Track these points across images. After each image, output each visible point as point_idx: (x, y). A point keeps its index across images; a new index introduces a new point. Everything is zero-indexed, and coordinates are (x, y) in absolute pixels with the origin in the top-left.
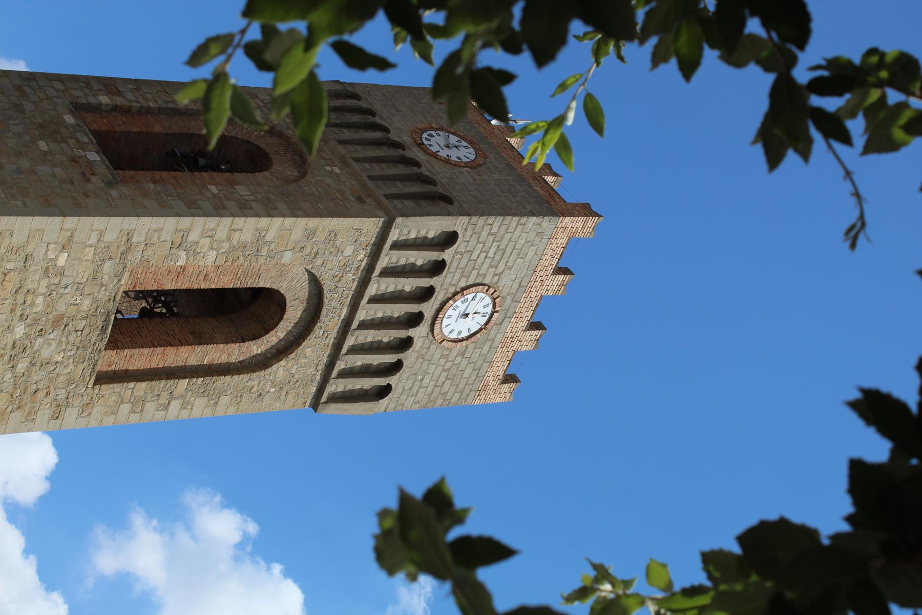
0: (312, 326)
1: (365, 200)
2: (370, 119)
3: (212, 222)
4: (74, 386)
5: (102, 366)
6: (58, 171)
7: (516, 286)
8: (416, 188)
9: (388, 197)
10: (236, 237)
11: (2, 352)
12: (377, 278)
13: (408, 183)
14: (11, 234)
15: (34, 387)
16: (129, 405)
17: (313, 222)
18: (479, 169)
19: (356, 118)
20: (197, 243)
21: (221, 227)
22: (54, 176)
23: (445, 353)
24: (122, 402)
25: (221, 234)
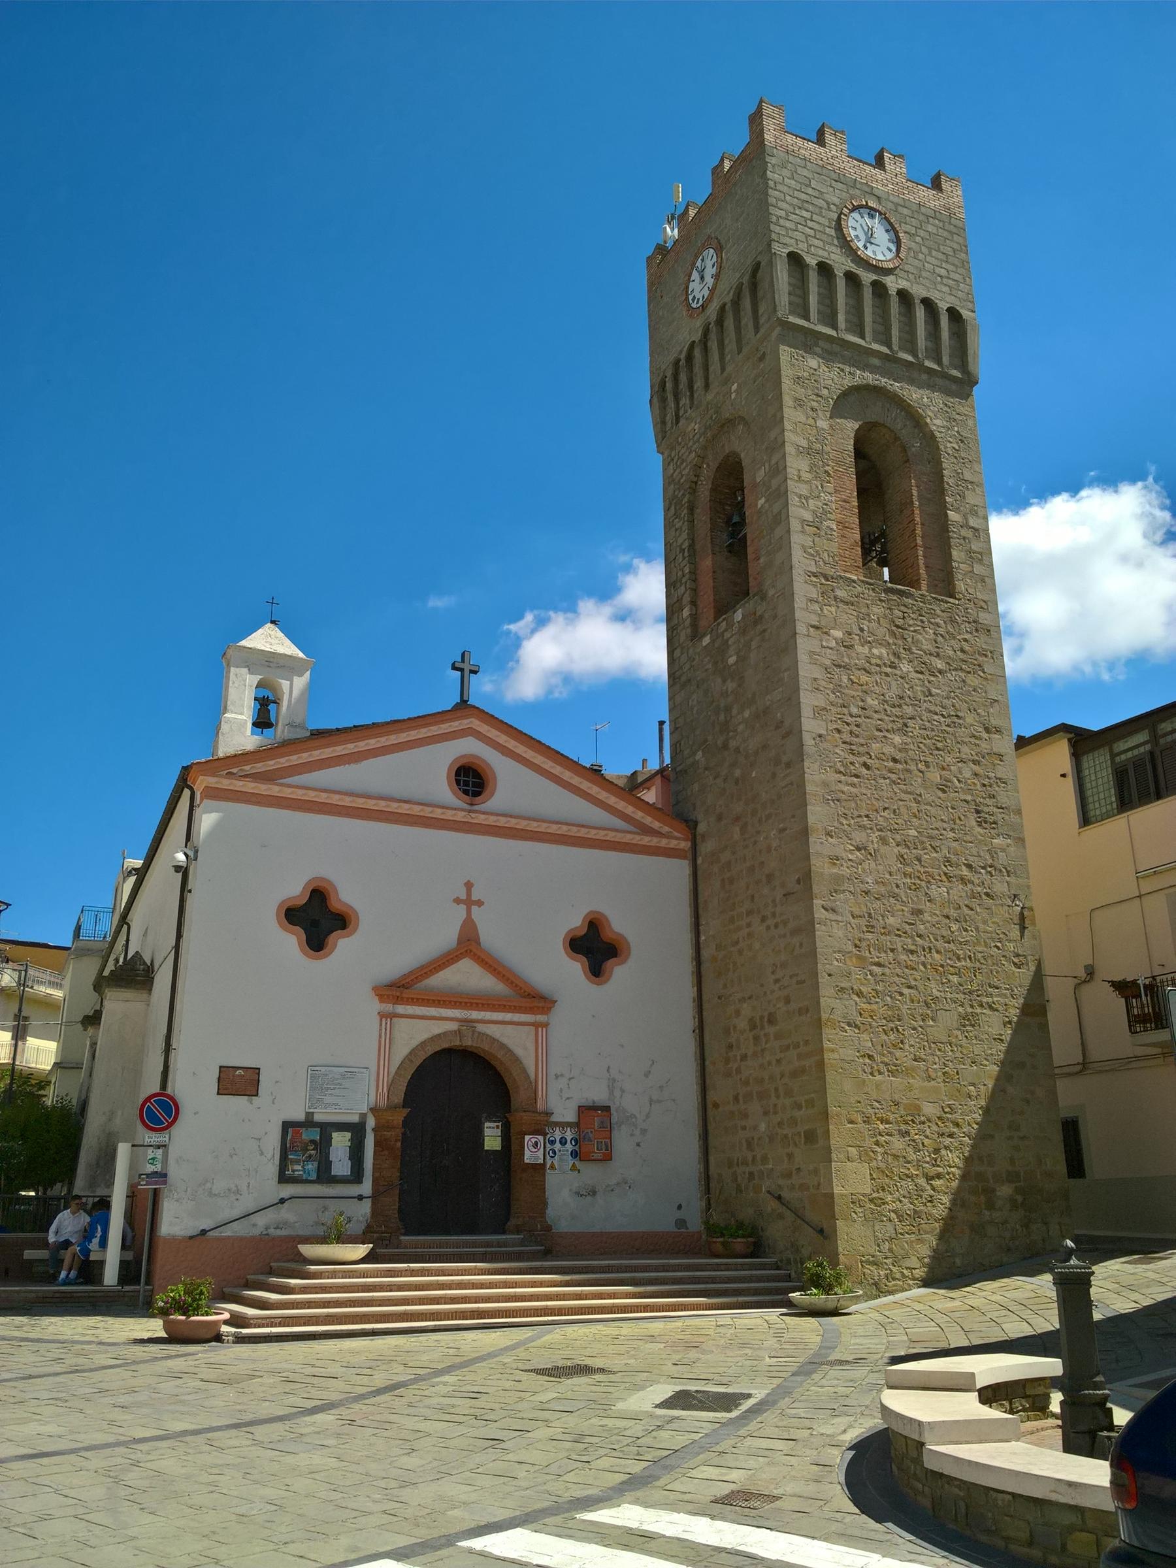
0: (890, 394)
1: (762, 353)
2: (683, 362)
3: (793, 500)
4: (957, 617)
7: (839, 185)
8: (747, 303)
9: (757, 329)
10: (806, 476)
12: (839, 331)
13: (742, 313)
14: (815, 679)
15: (959, 653)
16: (975, 565)
17: (787, 400)
18: (723, 242)
19: (683, 377)
20: (814, 512)
21: (797, 490)
22: (759, 647)
23: (912, 255)
24: (972, 572)
25: (804, 490)
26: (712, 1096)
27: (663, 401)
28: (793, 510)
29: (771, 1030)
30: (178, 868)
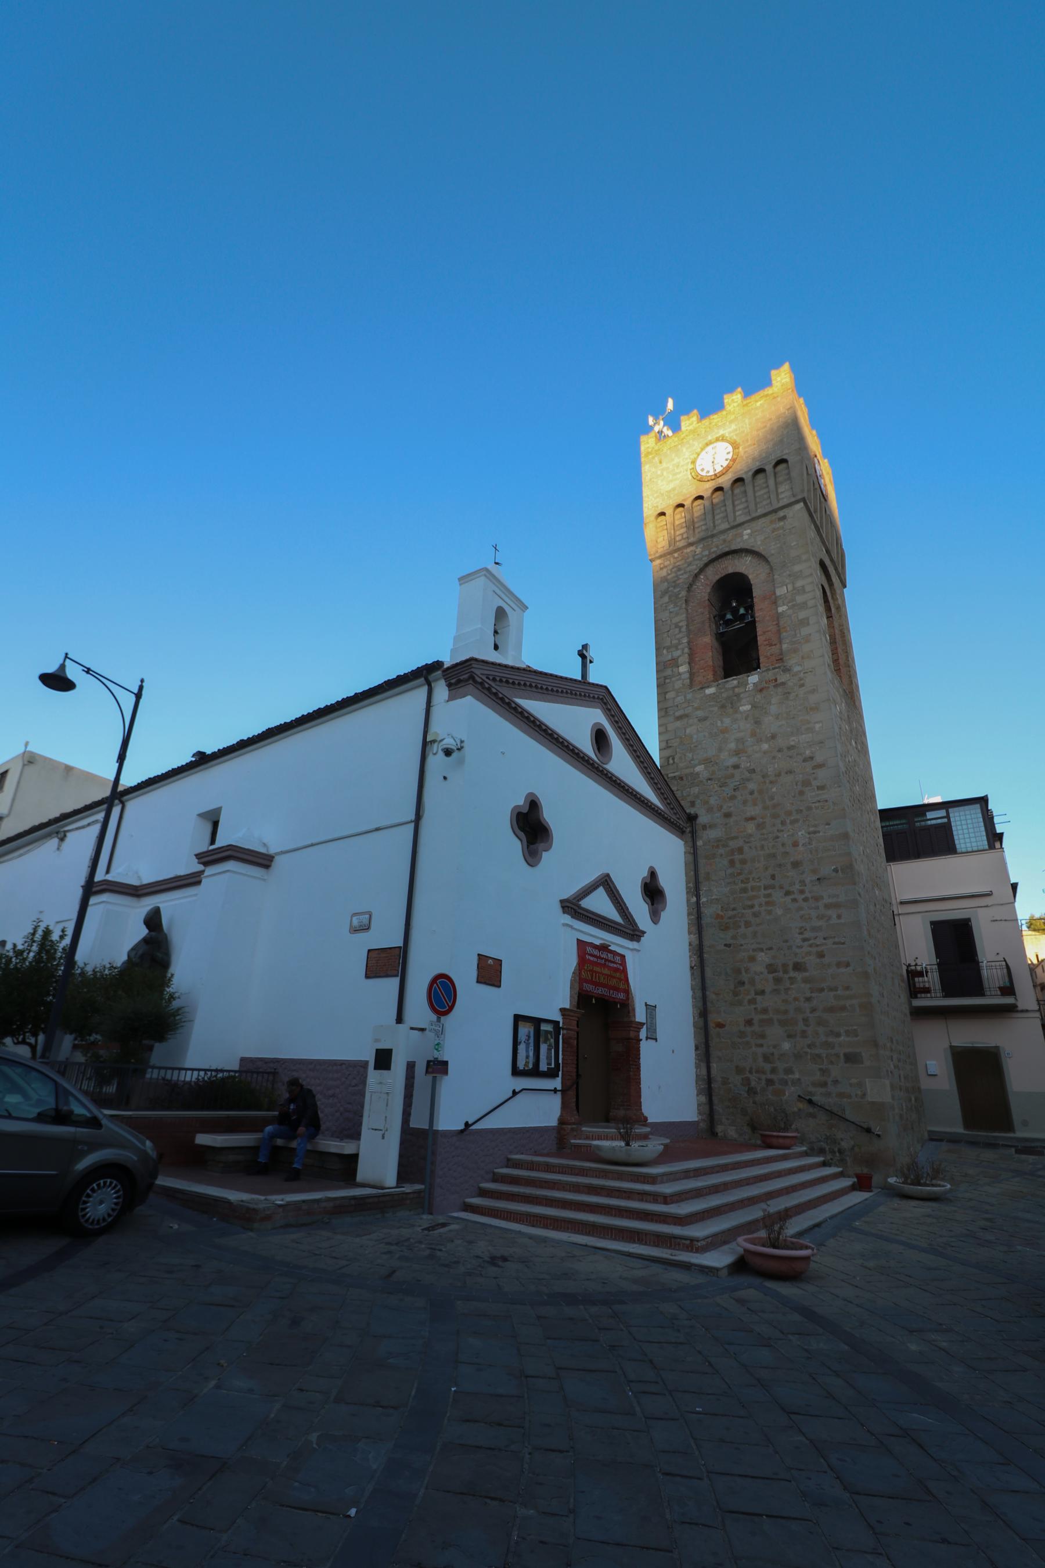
6: (774, 700)
26: (713, 1018)
29: (799, 976)
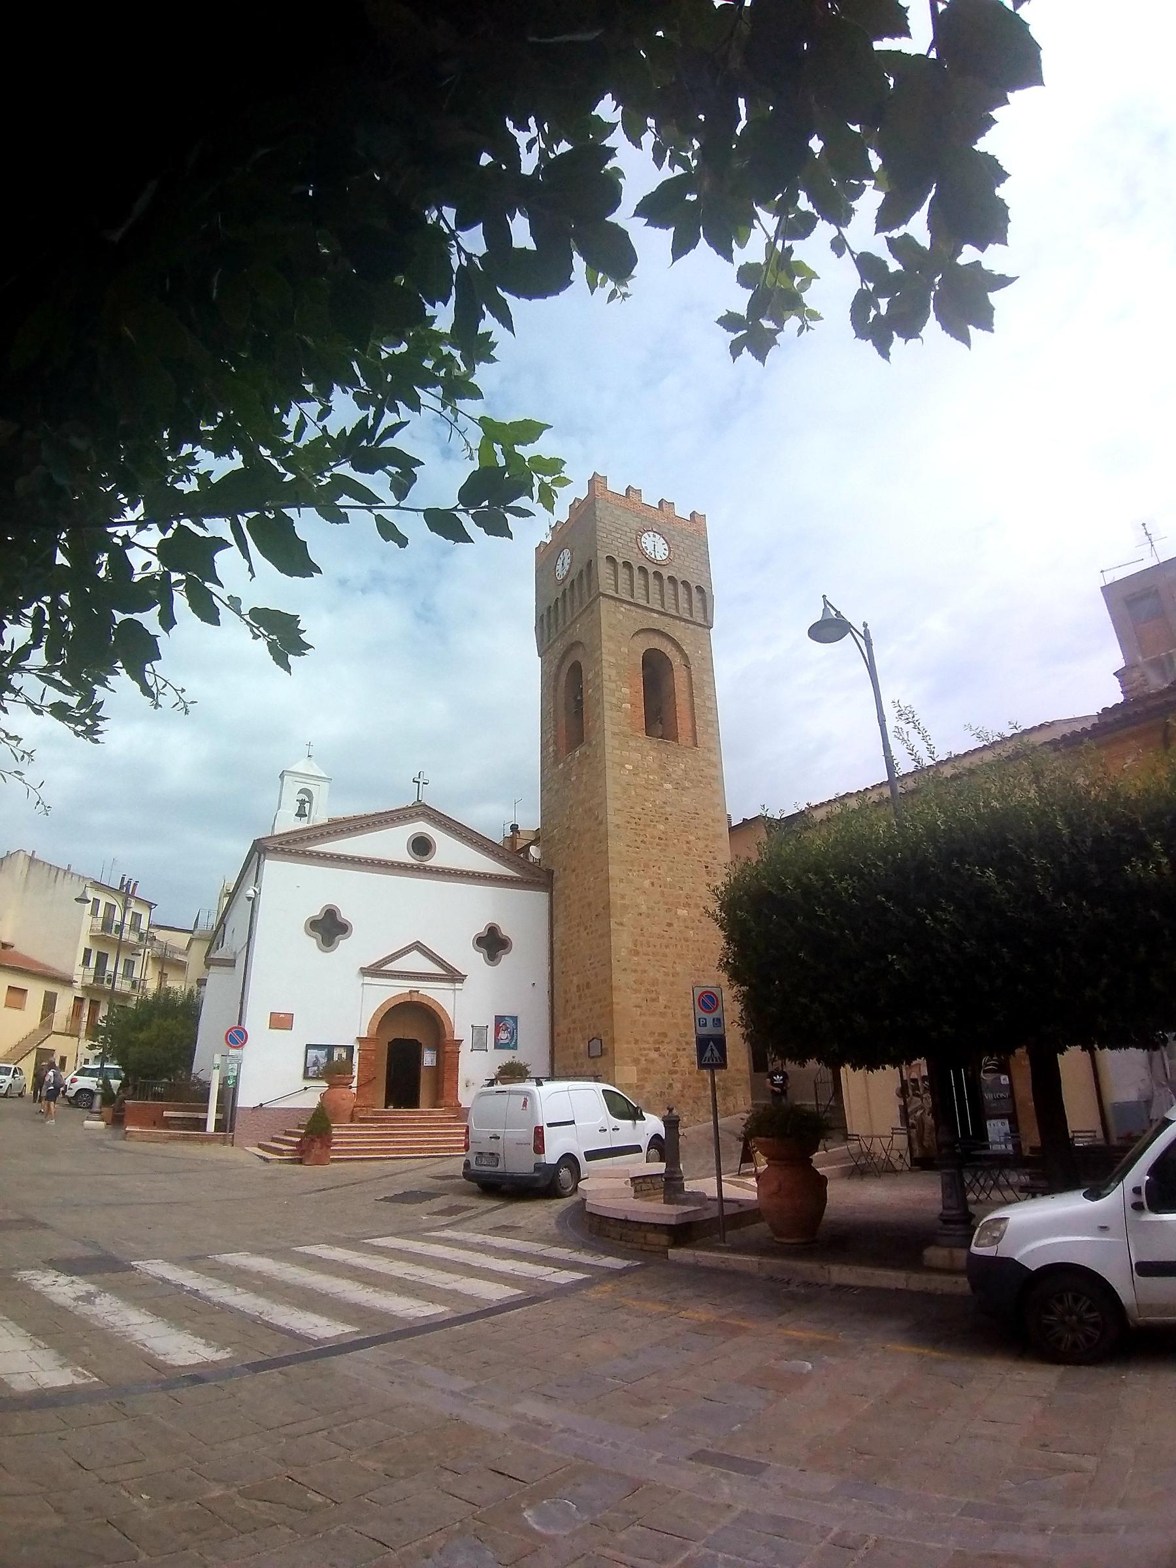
5: (690, 743)
11: (2, 1085)
19: (552, 614)
27: (542, 628)
28: (605, 698)
29: (586, 991)
30: (249, 899)
